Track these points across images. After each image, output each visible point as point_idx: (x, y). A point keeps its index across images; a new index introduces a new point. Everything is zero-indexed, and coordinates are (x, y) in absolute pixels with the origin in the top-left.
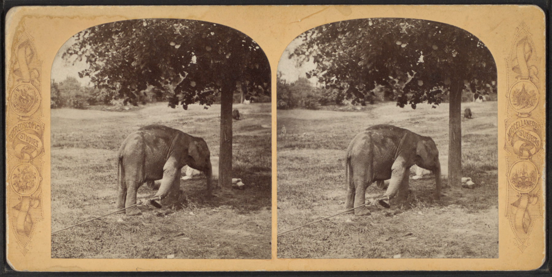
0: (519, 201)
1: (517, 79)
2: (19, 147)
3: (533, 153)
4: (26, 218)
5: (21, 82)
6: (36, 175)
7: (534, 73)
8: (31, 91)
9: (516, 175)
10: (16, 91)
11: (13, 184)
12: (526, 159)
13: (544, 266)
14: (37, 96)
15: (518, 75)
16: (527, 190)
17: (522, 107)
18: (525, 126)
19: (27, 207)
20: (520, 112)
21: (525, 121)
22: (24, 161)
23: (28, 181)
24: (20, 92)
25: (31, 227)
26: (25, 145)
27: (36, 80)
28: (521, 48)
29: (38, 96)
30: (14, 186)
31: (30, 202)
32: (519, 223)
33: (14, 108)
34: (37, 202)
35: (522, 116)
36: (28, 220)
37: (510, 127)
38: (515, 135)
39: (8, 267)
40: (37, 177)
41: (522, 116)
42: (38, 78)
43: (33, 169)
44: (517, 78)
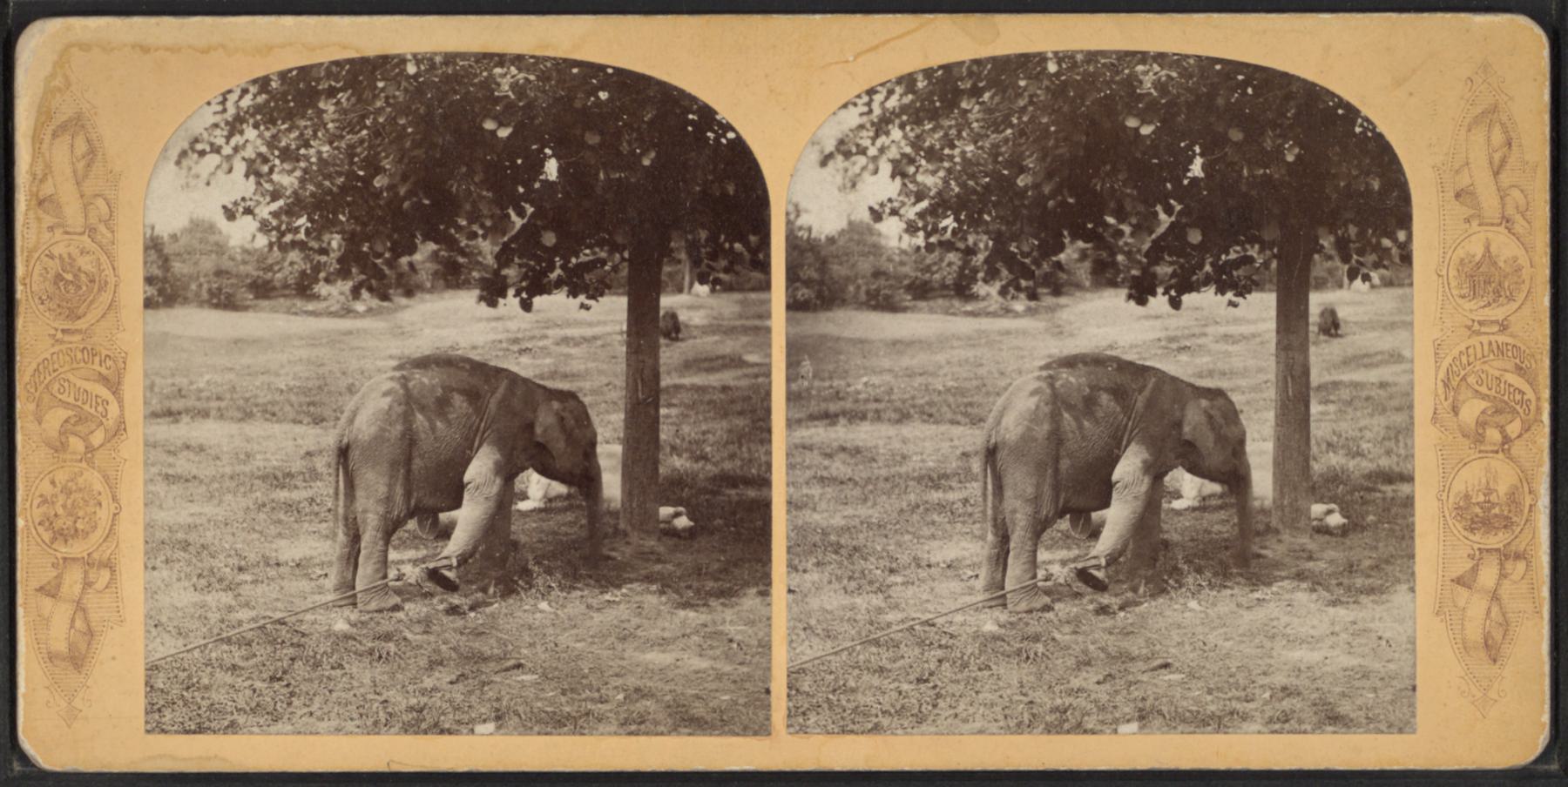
0: (1475, 570)
2: (55, 418)
3: (1513, 436)
4: (73, 620)
6: (102, 499)
7: (1517, 208)
8: (87, 258)
11: (37, 521)
12: (1492, 452)
13: (1544, 757)
16: (1496, 540)
17: (1482, 304)
18: (1492, 356)
19: (77, 588)
23: (81, 514)
24: (57, 261)
26: (70, 413)
27: (102, 228)
28: (1479, 136)
29: (109, 272)
30: (41, 529)
31: (86, 573)
32: (1474, 632)
33: (41, 307)
34: (105, 575)
35: (1483, 329)
36: (79, 624)
38: (1463, 383)
39: (24, 758)
40: (104, 504)
41: (1483, 329)
42: (109, 221)
43: (94, 479)
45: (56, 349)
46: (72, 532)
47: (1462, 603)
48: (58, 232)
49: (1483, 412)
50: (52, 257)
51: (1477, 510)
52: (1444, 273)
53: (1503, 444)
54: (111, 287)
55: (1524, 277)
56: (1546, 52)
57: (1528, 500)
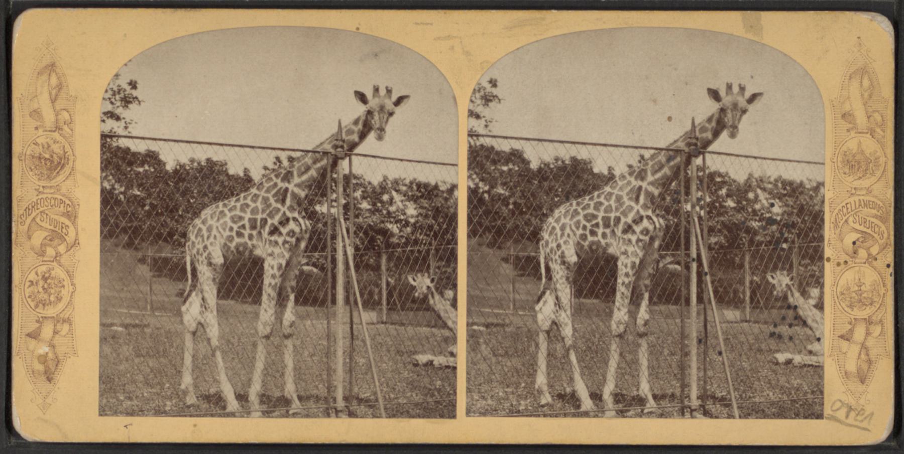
0: (851, 331)
1: (36, 132)
2: (38, 237)
4: (860, 354)
6: (65, 283)
7: (877, 124)
8: (57, 145)
9: (849, 289)
10: (34, 146)
11: (27, 295)
12: (49, 261)
13: (889, 439)
14: (68, 153)
15: (851, 126)
16: (865, 313)
17: (856, 178)
18: (861, 208)
20: (42, 185)
21: (860, 200)
23: (53, 291)
24: (41, 147)
26: (859, 235)
27: (878, 130)
28: (855, 84)
29: (70, 153)
30: (29, 300)
31: (55, 325)
32: (852, 367)
33: (31, 173)
34: (66, 327)
36: (863, 356)
37: (836, 211)
38: (34, 223)
39: (17, 436)
42: (69, 123)
43: (58, 272)
44: (36, 128)
48: (853, 134)
49: (45, 238)
51: (854, 295)
52: (835, 160)
55: (880, 163)
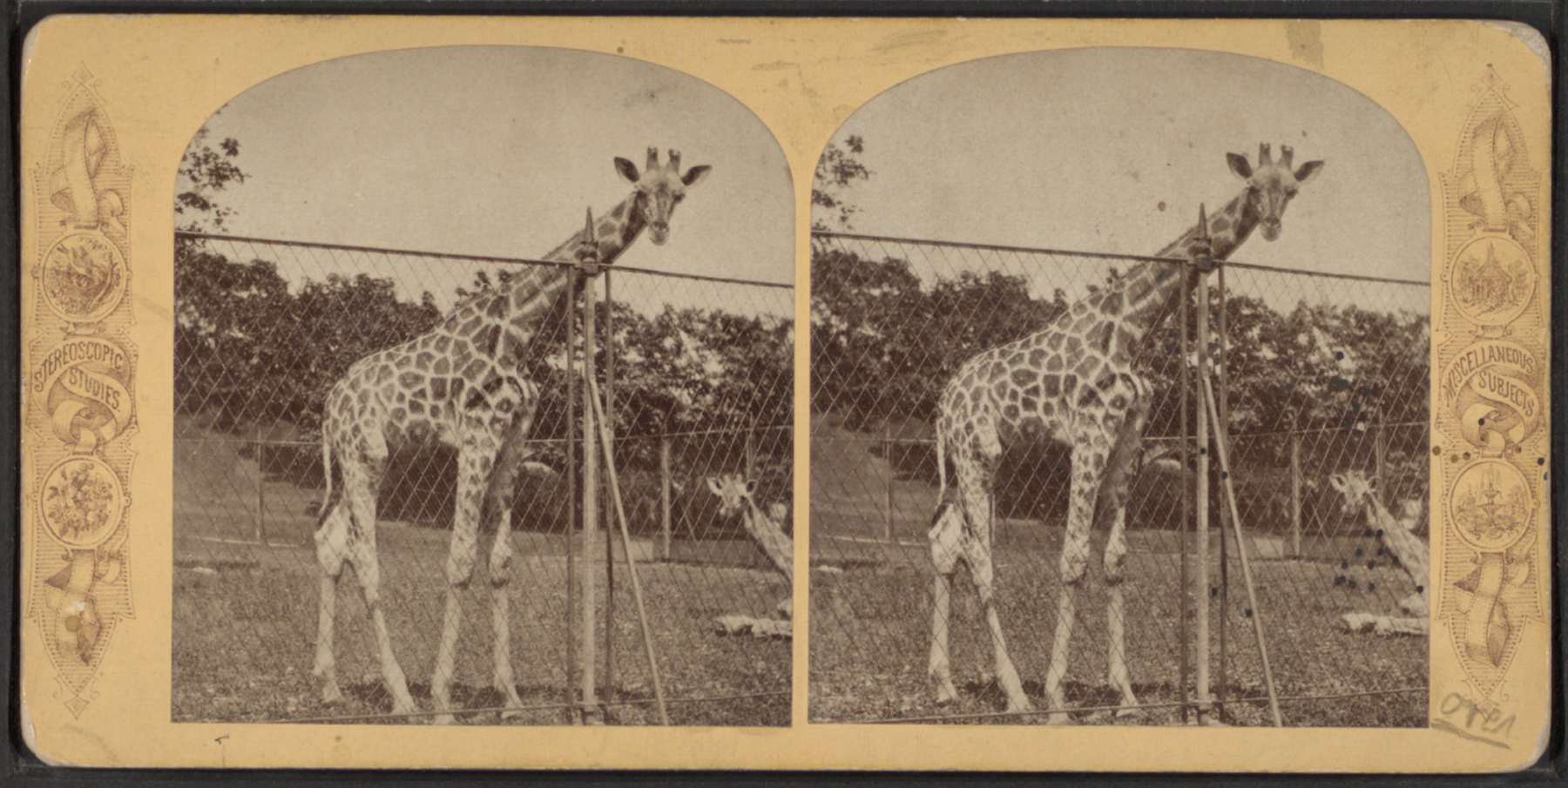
0: (1477, 574)
1: (63, 228)
2: (66, 412)
3: (108, 438)
4: (1492, 614)
5: (1479, 232)
6: (113, 492)
11: (47, 514)
13: (1541, 762)
14: (118, 266)
15: (1476, 218)
17: (1485, 308)
18: (1493, 362)
19: (88, 579)
20: (72, 320)
22: (1487, 452)
23: (91, 505)
24: (71, 255)
25: (98, 634)
26: (1490, 409)
27: (1523, 226)
28: (1483, 146)
29: (121, 265)
30: (51, 521)
32: (1477, 637)
33: (54, 301)
34: (114, 568)
35: (1488, 335)
36: (1497, 619)
39: (30, 756)
40: (115, 498)
41: (1488, 335)
42: (120, 214)
43: (101, 472)
44: (63, 223)
45: (70, 341)
46: (83, 523)
47: (1464, 607)
48: (70, 229)
50: (62, 250)
53: (97, 446)
54: (123, 282)
56: (1548, 57)
57: (1186, 506)
